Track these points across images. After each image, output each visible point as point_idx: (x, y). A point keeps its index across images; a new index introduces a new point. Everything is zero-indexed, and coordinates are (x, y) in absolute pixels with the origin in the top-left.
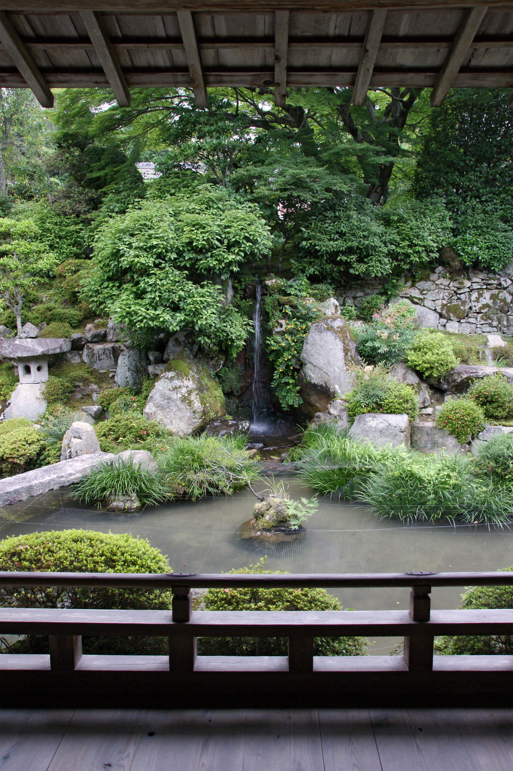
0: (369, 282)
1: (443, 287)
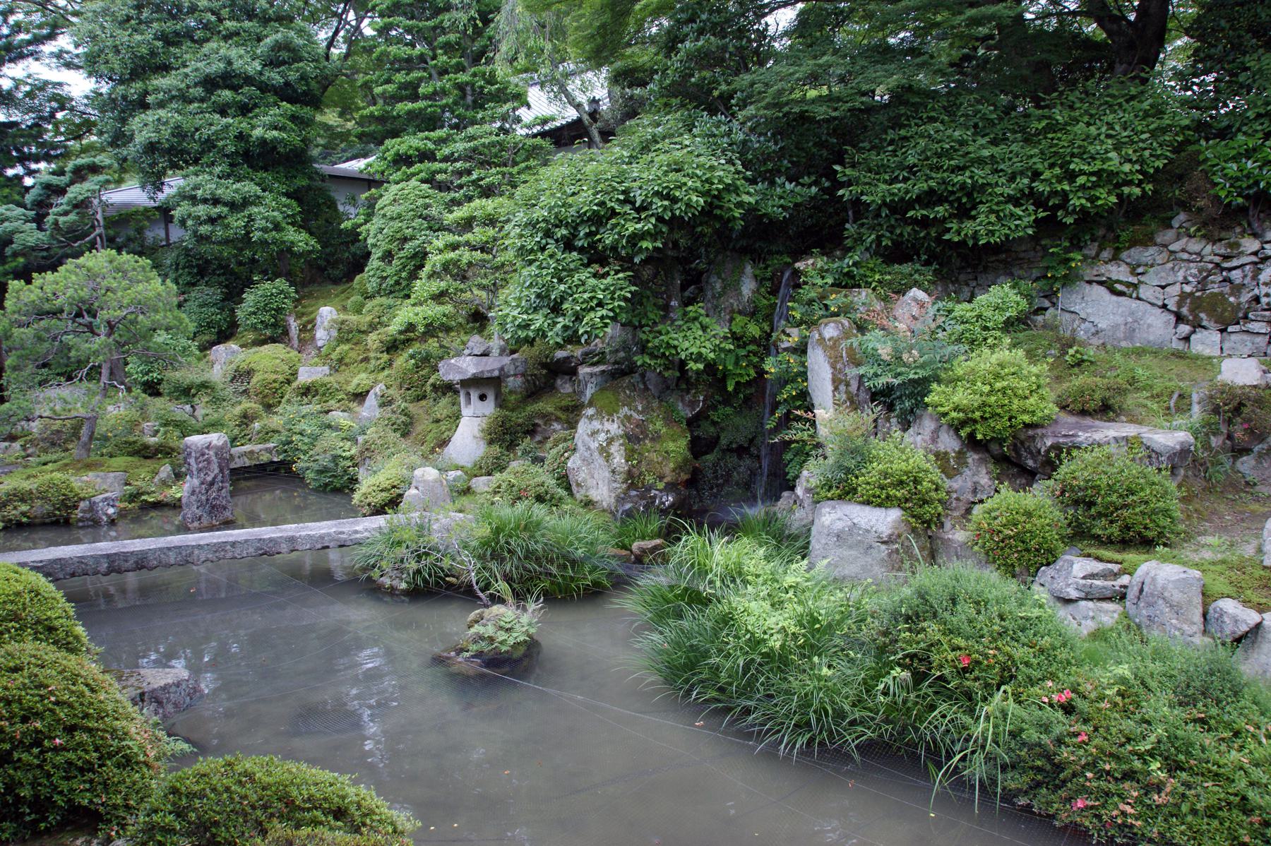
0: (1022, 255)
1: (1185, 256)
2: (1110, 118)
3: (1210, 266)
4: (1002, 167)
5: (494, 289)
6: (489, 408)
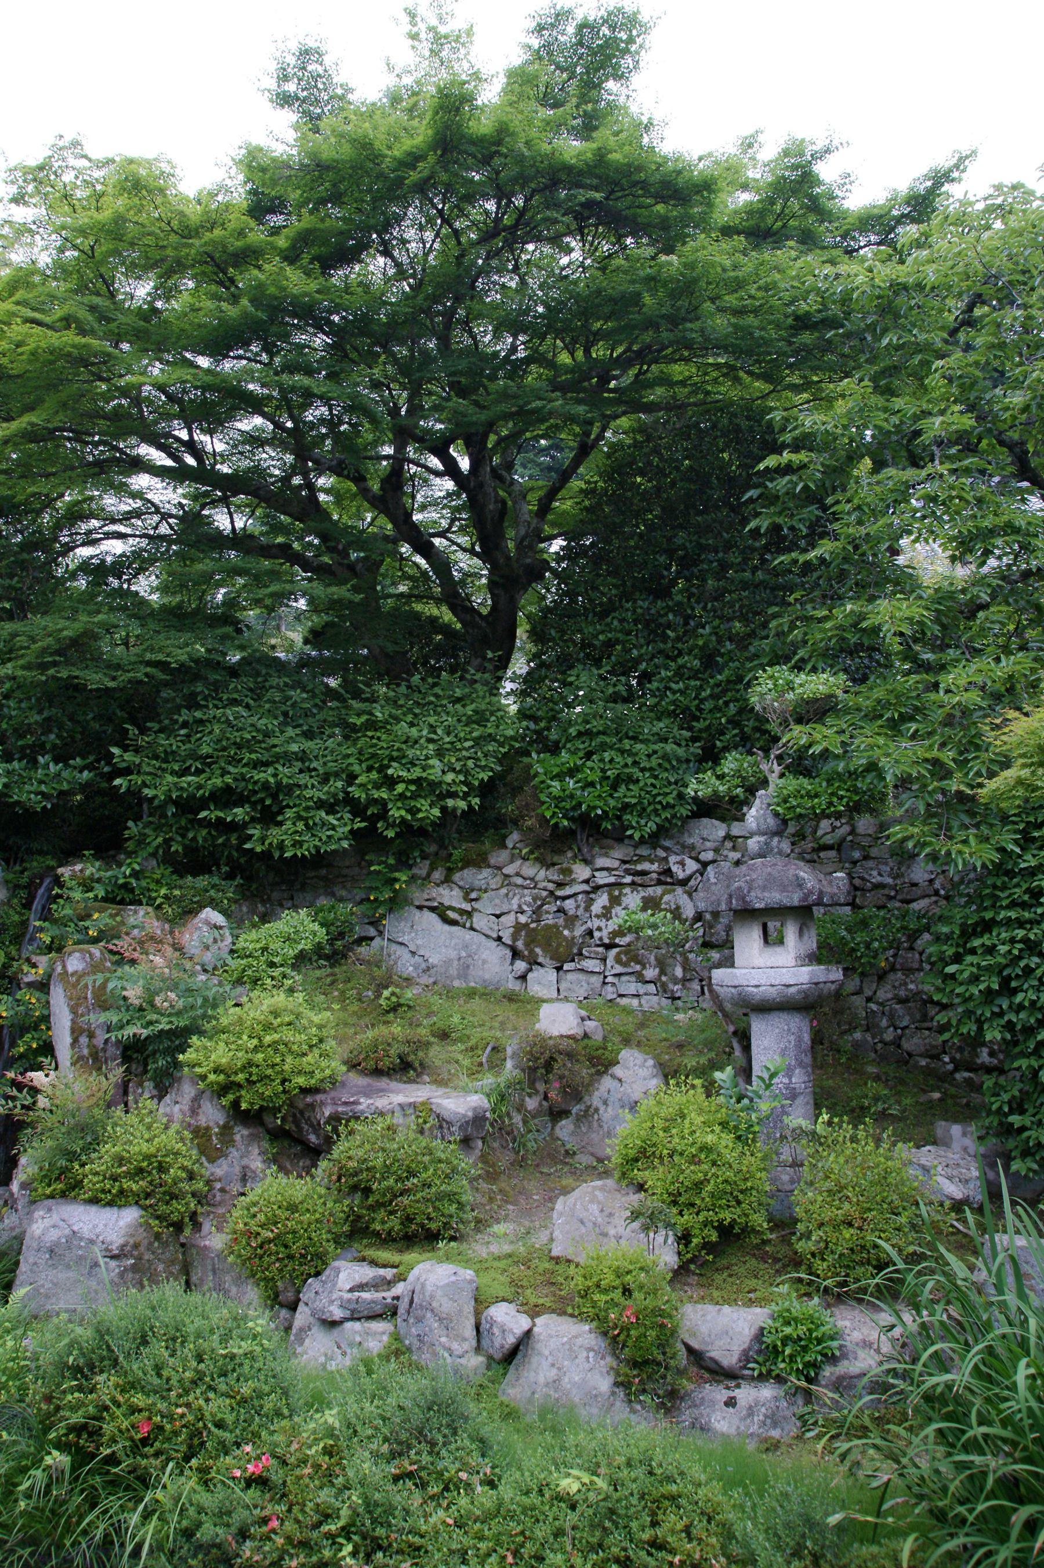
0: (345, 871)
1: (519, 881)
2: (432, 720)
3: (545, 894)
4: (314, 764)
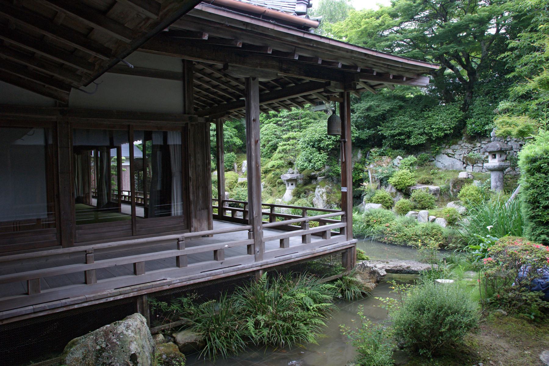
5: (295, 156)
6: (294, 187)
